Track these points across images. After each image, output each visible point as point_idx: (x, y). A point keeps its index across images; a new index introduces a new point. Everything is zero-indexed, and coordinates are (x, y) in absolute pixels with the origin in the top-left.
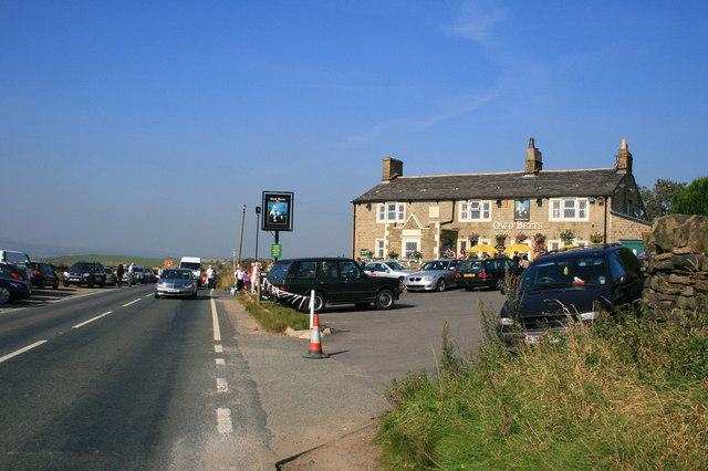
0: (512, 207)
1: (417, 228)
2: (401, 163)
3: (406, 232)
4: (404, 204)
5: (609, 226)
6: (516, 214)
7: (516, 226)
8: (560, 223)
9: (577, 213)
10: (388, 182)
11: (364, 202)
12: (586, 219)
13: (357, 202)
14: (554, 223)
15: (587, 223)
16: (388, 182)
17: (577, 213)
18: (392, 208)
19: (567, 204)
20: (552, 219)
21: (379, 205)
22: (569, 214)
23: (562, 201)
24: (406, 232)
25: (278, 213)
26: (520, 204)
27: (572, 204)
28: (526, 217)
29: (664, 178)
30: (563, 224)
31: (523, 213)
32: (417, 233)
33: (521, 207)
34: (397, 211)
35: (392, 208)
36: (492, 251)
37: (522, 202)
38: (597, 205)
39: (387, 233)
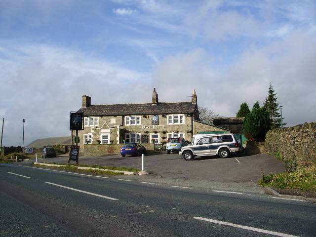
0: (151, 119)
3: (102, 131)
9: (179, 121)
12: (183, 123)
17: (179, 121)
19: (175, 117)
24: (102, 131)
26: (154, 117)
28: (157, 123)
32: (109, 131)
33: (154, 118)
39: (93, 131)
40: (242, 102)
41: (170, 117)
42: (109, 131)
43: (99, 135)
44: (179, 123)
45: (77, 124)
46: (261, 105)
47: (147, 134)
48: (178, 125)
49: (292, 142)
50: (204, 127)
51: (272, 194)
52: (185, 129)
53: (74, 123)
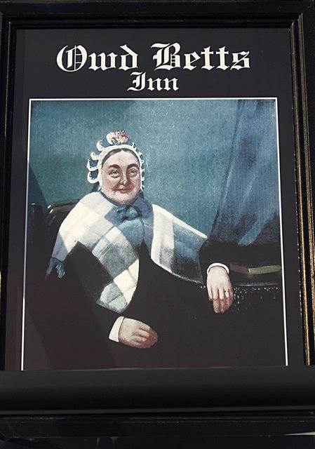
25: (166, 232)
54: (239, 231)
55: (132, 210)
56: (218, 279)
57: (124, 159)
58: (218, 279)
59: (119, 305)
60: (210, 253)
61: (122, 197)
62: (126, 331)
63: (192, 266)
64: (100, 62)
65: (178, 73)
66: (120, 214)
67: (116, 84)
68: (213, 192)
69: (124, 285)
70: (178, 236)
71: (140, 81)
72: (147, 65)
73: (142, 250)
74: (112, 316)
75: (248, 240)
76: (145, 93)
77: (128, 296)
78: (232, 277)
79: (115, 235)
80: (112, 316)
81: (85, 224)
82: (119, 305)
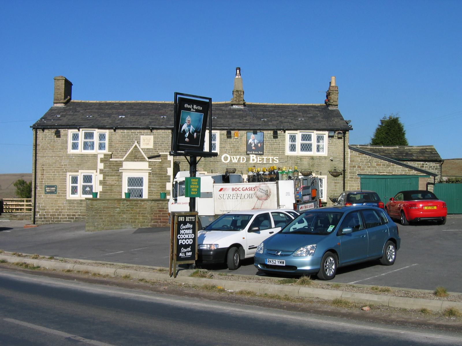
0: (244, 139)
1: (142, 159)
2: (211, 98)
3: (127, 165)
4: (107, 132)
5: (348, 161)
6: (249, 147)
7: (248, 160)
8: (297, 157)
9: (96, 146)
10: (62, 105)
11: (51, 127)
12: (324, 153)
13: (39, 127)
14: (291, 157)
15: (325, 158)
16: (62, 105)
17: (314, 147)
18: (89, 136)
19: (304, 138)
20: (288, 152)
21: (71, 132)
22: (306, 147)
23: (299, 134)
24: (127, 165)
25: (256, 141)
26: (253, 136)
27: (309, 138)
28: (259, 150)
29: (401, 121)
30: (301, 158)
31: (256, 146)
32: (145, 165)
33: (253, 139)
34: (96, 139)
35: (89, 136)
36: (203, 189)
37: (255, 133)
38: (335, 140)
39: (101, 166)
40: (388, 114)
41: (293, 138)
42: (145, 165)
43: (120, 176)
44: (314, 153)
45: (191, 136)
46: (380, 124)
47: (400, 210)
48: (312, 158)
49: (211, 163)
50: (375, 164)
51: (356, 283)
52: (327, 167)
53: (251, 144)
54: (198, 129)
55: (189, 126)
56: (259, 145)
57: (189, 119)
58: (259, 145)
59: (186, 137)
60: (259, 143)
61: (188, 124)
62: (187, 140)
63: (258, 144)
64: (189, 107)
65: (195, 109)
66: (253, 140)
67: (189, 109)
68: (196, 124)
69: (253, 145)
70: (193, 129)
71: (192, 110)
72: (193, 108)
73: (254, 143)
74: (186, 138)
75: (198, 130)
76: (192, 111)
77: (187, 135)
78: (197, 135)
79: (253, 142)
80: (186, 138)
81: (185, 127)
82: (186, 137)
